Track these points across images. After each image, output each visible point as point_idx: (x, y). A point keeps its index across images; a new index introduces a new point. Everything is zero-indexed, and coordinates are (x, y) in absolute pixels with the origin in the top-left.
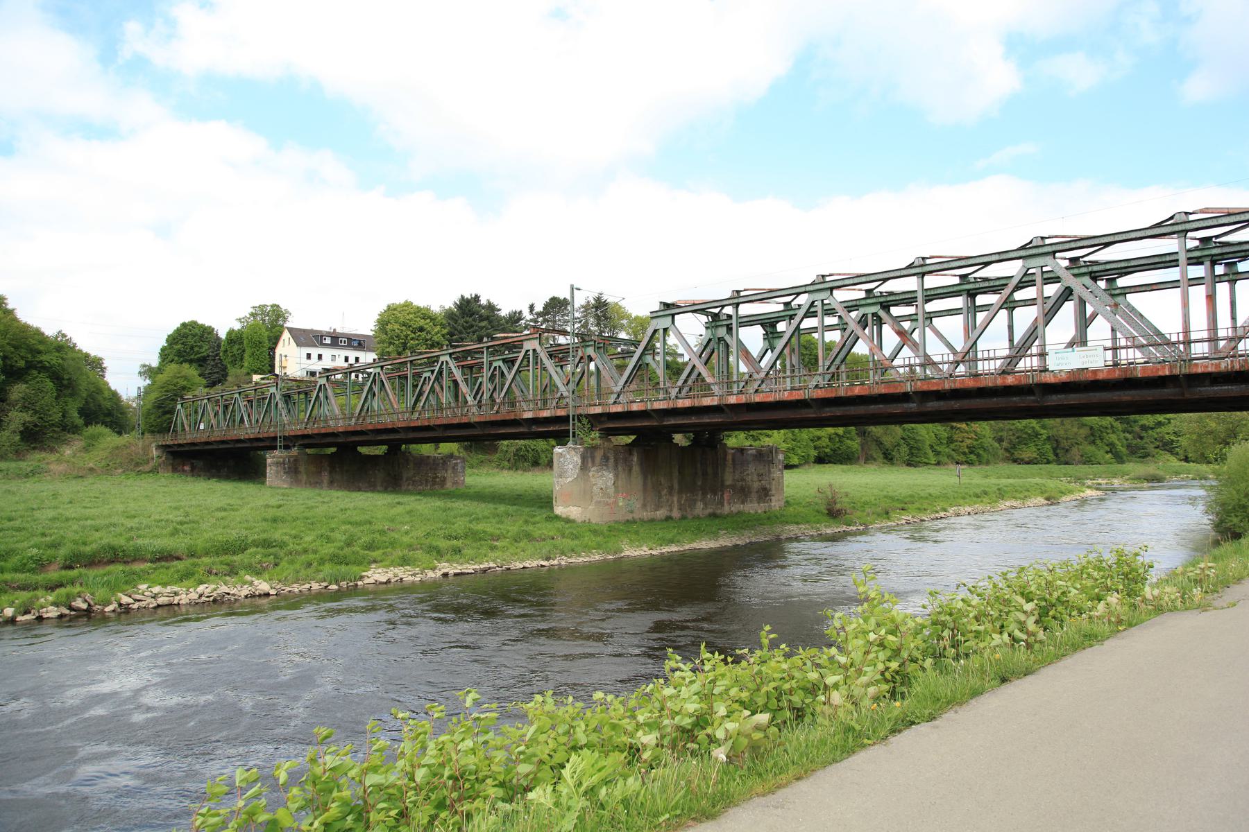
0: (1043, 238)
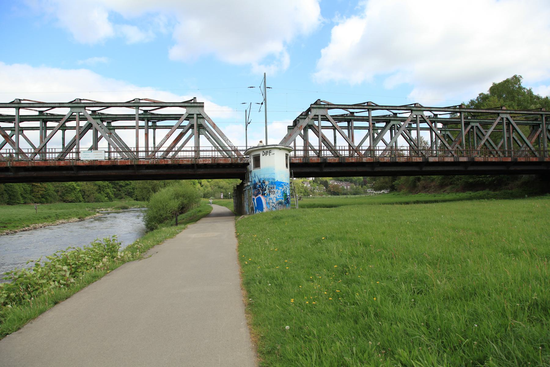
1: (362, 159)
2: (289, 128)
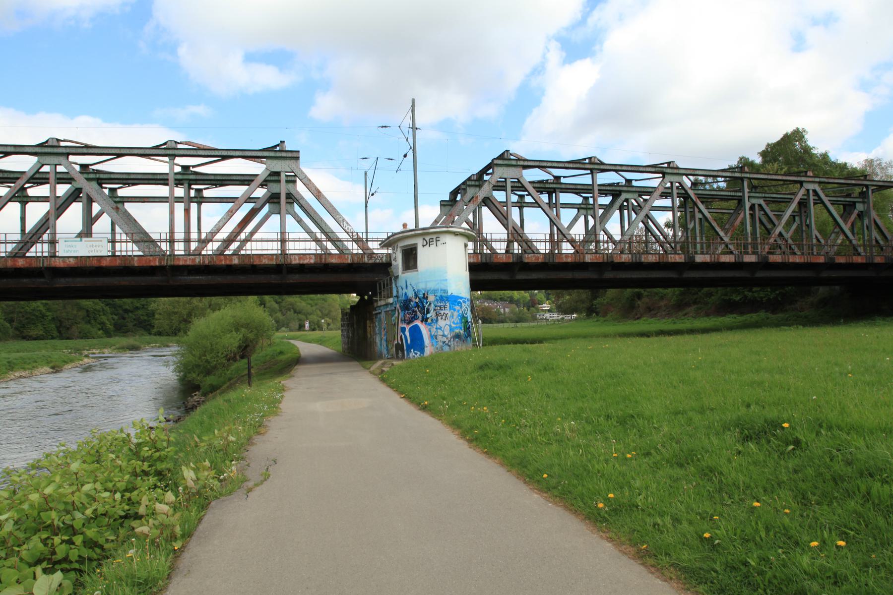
0: (58, 140)
1: (584, 257)
2: (443, 204)
